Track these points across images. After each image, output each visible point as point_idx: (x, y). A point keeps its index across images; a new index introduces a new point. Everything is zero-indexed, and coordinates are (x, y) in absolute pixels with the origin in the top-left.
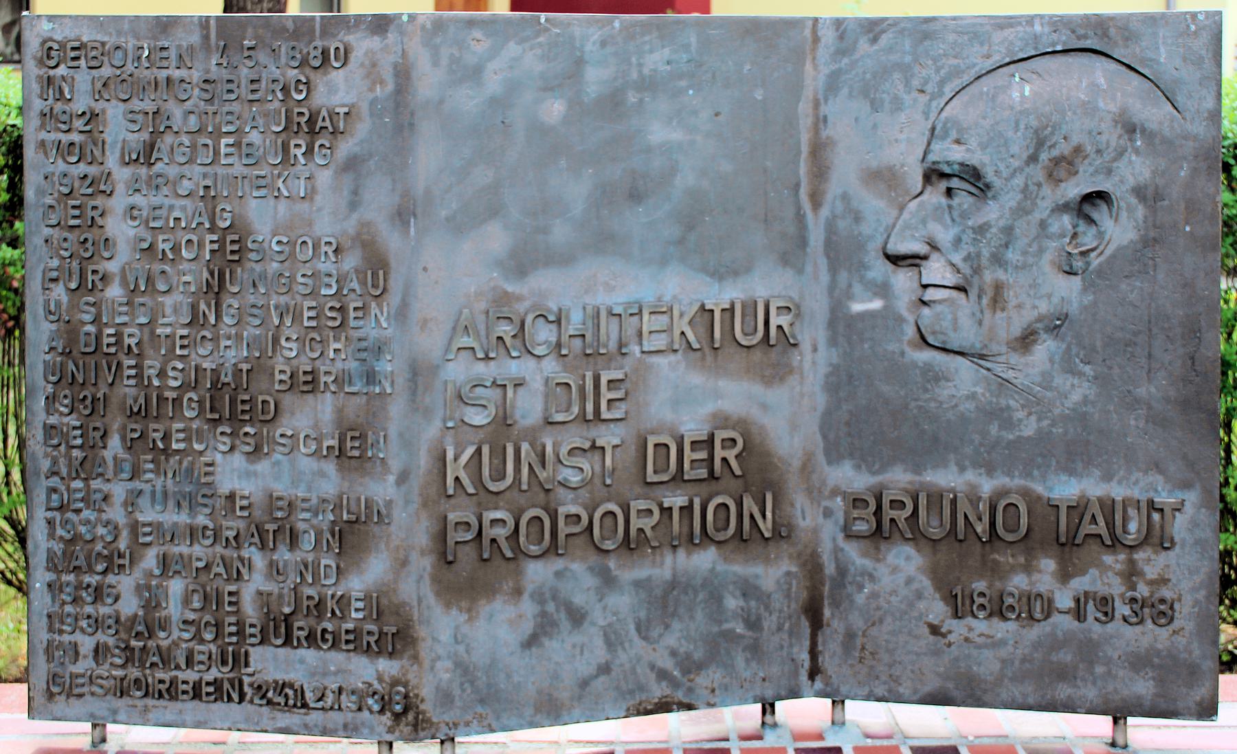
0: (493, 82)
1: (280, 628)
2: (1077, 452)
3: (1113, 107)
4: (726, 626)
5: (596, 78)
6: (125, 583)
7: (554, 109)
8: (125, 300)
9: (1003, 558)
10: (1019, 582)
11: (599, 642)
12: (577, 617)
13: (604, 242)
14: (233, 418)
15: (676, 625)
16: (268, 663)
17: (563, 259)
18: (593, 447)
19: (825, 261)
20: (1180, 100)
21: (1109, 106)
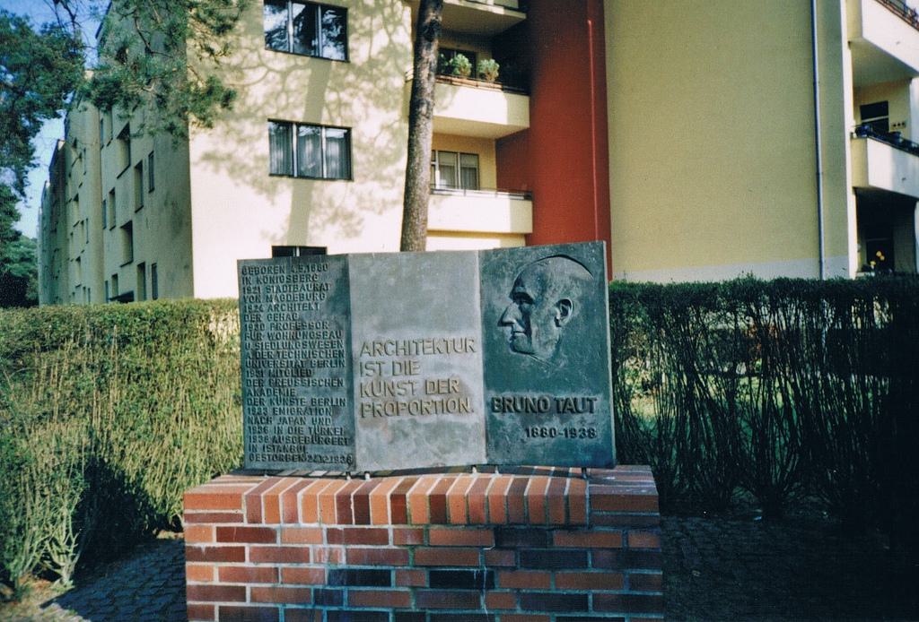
0: (373, 272)
1: (316, 439)
2: (558, 382)
3: (569, 273)
4: (456, 440)
5: (405, 272)
6: (270, 427)
7: (392, 281)
8: (390, 87)
9: (543, 417)
10: (547, 426)
11: (414, 444)
12: (406, 435)
13: (412, 321)
14: (302, 376)
15: (439, 439)
16: (312, 450)
17: (397, 326)
18: (409, 382)
19: (854, 197)
20: (591, 269)
21: (568, 273)
